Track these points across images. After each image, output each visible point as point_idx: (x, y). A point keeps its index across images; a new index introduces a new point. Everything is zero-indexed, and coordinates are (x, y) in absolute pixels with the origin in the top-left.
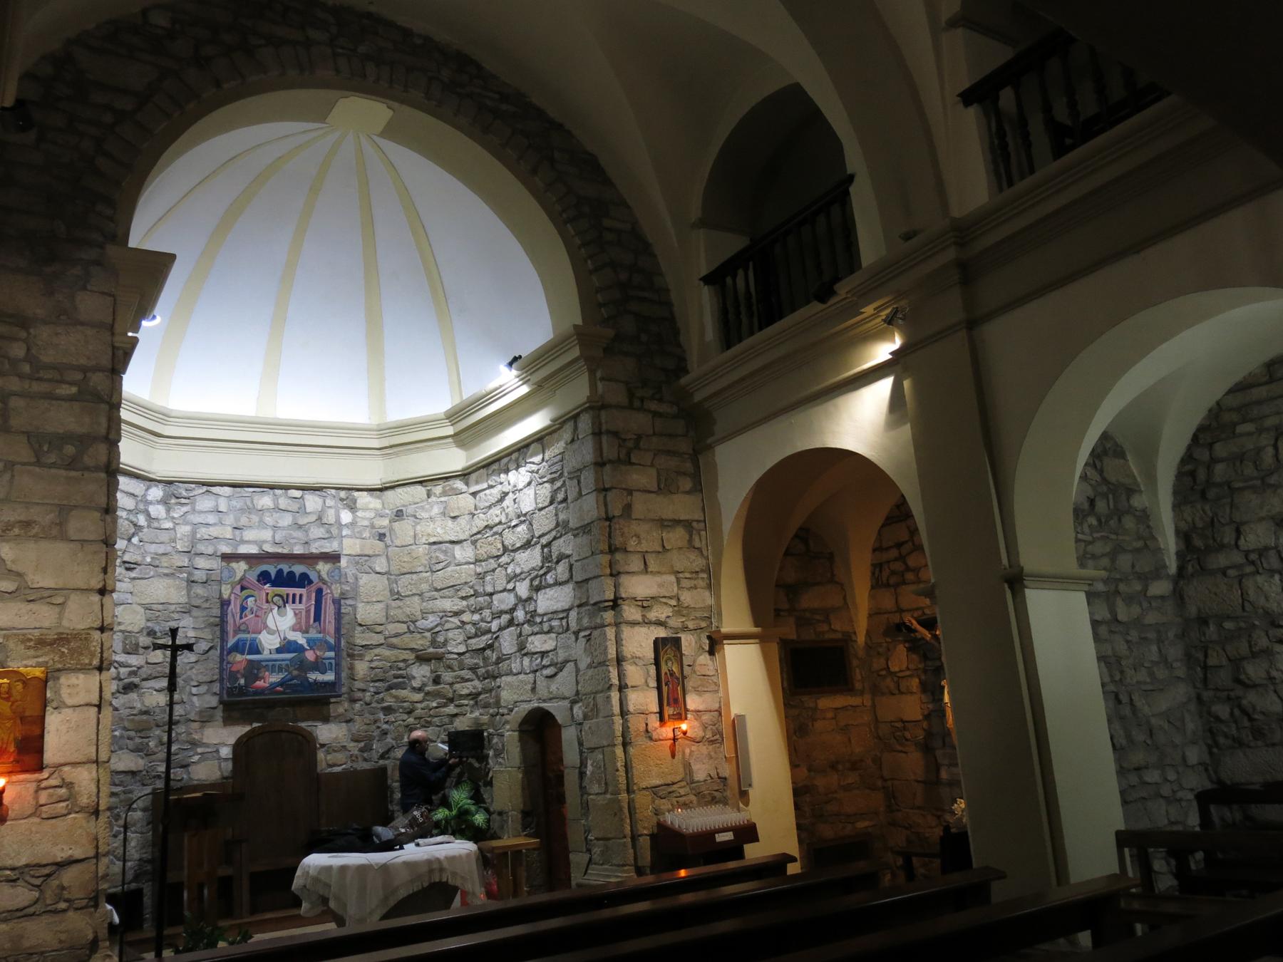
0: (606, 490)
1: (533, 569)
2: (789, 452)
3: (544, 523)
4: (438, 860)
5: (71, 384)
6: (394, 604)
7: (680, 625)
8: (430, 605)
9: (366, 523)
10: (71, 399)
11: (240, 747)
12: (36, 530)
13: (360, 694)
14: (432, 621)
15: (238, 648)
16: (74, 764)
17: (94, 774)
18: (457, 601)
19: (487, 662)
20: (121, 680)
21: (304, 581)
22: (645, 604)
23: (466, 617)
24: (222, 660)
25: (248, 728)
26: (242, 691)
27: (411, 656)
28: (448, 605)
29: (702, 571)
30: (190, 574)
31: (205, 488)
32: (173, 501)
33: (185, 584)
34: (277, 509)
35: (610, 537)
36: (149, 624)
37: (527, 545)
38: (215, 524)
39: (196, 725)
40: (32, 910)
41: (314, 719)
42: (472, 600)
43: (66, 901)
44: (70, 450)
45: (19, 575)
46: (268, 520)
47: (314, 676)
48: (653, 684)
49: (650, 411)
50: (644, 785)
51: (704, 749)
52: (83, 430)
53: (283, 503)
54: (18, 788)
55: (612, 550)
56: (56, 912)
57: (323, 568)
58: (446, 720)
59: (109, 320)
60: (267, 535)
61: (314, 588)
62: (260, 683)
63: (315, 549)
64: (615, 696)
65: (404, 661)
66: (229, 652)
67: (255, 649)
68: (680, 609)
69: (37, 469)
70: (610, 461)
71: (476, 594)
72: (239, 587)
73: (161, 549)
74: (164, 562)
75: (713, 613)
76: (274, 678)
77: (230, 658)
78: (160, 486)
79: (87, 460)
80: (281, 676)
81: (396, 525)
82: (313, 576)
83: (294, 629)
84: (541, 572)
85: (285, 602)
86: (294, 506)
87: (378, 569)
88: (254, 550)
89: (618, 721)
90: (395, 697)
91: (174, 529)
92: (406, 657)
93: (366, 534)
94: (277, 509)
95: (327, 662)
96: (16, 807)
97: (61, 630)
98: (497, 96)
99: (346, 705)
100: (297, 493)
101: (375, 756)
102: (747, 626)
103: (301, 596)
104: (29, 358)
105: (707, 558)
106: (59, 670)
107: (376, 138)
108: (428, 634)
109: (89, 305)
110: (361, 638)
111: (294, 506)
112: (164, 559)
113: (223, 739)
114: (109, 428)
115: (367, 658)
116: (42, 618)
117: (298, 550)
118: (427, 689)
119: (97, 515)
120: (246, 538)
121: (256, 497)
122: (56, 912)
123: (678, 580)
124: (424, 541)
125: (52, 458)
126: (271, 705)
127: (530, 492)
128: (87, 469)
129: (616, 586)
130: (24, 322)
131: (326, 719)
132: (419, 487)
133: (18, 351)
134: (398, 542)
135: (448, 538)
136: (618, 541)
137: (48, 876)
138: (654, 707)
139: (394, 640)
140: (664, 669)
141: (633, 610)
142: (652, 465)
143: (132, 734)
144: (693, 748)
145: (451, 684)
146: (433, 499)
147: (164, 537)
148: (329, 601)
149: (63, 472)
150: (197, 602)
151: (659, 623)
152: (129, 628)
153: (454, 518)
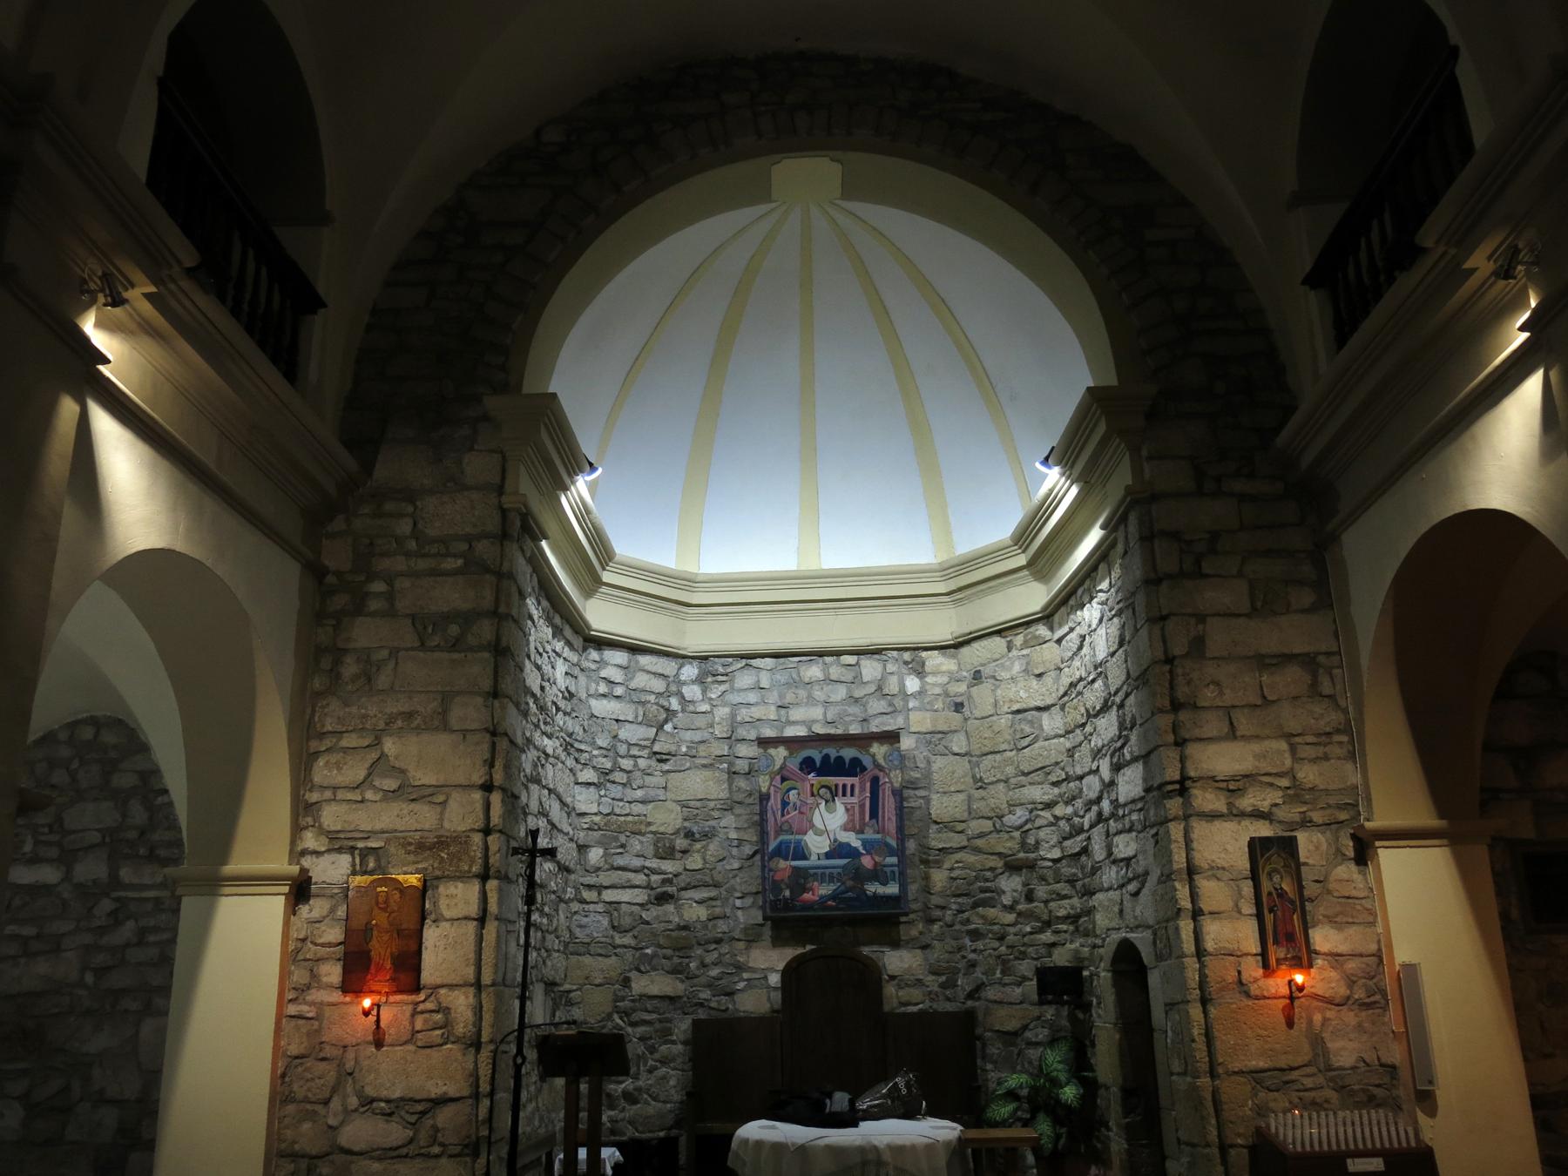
0: (1164, 618)
1: (1112, 740)
2: (1424, 528)
3: (1116, 675)
4: (875, 1148)
5: (455, 556)
6: (978, 794)
7: (1297, 818)
9: (938, 690)
11: (791, 973)
12: (418, 721)
13: (938, 913)
14: (1019, 816)
15: (781, 852)
16: (451, 987)
17: (471, 1000)
18: (1047, 787)
19: (1079, 873)
22: (1233, 786)
23: (1060, 810)
24: (763, 867)
25: (800, 951)
26: (788, 905)
27: (1000, 864)
28: (1039, 793)
29: (1338, 731)
30: (731, 764)
31: (744, 662)
32: (710, 679)
34: (828, 680)
35: (1172, 687)
36: (687, 824)
37: (1105, 708)
39: (741, 945)
40: (404, 1151)
41: (881, 944)
43: (442, 1145)
44: (454, 630)
45: (403, 772)
46: (818, 694)
47: (873, 888)
48: (1249, 908)
50: (1237, 1066)
51: (1350, 1017)
53: (835, 672)
54: (395, 1009)
55: (1176, 706)
56: (428, 1156)
57: (879, 750)
58: (1043, 951)
59: (497, 480)
60: (817, 713)
61: (868, 776)
62: (807, 896)
63: (875, 727)
64: (1186, 927)
65: (992, 869)
66: (770, 859)
67: (801, 853)
68: (1296, 793)
70: (1170, 576)
71: (1068, 779)
73: (697, 736)
74: (702, 749)
75: (1354, 801)
76: (824, 890)
77: (772, 865)
78: (695, 663)
79: (471, 640)
80: (832, 887)
81: (974, 690)
82: (867, 761)
83: (845, 828)
84: (1119, 744)
85: (834, 794)
86: (849, 677)
87: (956, 749)
88: (801, 732)
89: (1192, 964)
90: (983, 917)
92: (992, 864)
93: (939, 705)
94: (828, 680)
95: (888, 870)
96: (392, 1031)
97: (442, 832)
100: (851, 659)
101: (962, 995)
102: (1422, 815)
103: (853, 786)
104: (416, 534)
105: (1345, 711)
106: (437, 878)
108: (1017, 834)
109: (477, 466)
110: (937, 840)
112: (702, 747)
113: (770, 962)
114: (497, 600)
115: (947, 865)
116: (418, 819)
117: (855, 729)
118: (1020, 907)
119: (479, 700)
120: (791, 719)
122: (428, 1156)
123: (1293, 749)
124: (1006, 709)
125: (436, 640)
126: (826, 923)
127: (1102, 631)
128: (471, 649)
129: (1182, 760)
130: (410, 495)
131: (896, 944)
132: (997, 639)
133: (405, 527)
134: (978, 714)
136: (1182, 692)
137: (423, 1113)
138: (1253, 946)
139: (979, 842)
140: (1266, 886)
141: (1210, 796)
142: (1240, 575)
143: (669, 952)
144: (1329, 1014)
145: (1046, 902)
146: (1014, 653)
147: (701, 721)
148: (888, 792)
149: (445, 655)
150: (739, 797)
151: (1257, 815)
152: (662, 829)
153: (1040, 676)
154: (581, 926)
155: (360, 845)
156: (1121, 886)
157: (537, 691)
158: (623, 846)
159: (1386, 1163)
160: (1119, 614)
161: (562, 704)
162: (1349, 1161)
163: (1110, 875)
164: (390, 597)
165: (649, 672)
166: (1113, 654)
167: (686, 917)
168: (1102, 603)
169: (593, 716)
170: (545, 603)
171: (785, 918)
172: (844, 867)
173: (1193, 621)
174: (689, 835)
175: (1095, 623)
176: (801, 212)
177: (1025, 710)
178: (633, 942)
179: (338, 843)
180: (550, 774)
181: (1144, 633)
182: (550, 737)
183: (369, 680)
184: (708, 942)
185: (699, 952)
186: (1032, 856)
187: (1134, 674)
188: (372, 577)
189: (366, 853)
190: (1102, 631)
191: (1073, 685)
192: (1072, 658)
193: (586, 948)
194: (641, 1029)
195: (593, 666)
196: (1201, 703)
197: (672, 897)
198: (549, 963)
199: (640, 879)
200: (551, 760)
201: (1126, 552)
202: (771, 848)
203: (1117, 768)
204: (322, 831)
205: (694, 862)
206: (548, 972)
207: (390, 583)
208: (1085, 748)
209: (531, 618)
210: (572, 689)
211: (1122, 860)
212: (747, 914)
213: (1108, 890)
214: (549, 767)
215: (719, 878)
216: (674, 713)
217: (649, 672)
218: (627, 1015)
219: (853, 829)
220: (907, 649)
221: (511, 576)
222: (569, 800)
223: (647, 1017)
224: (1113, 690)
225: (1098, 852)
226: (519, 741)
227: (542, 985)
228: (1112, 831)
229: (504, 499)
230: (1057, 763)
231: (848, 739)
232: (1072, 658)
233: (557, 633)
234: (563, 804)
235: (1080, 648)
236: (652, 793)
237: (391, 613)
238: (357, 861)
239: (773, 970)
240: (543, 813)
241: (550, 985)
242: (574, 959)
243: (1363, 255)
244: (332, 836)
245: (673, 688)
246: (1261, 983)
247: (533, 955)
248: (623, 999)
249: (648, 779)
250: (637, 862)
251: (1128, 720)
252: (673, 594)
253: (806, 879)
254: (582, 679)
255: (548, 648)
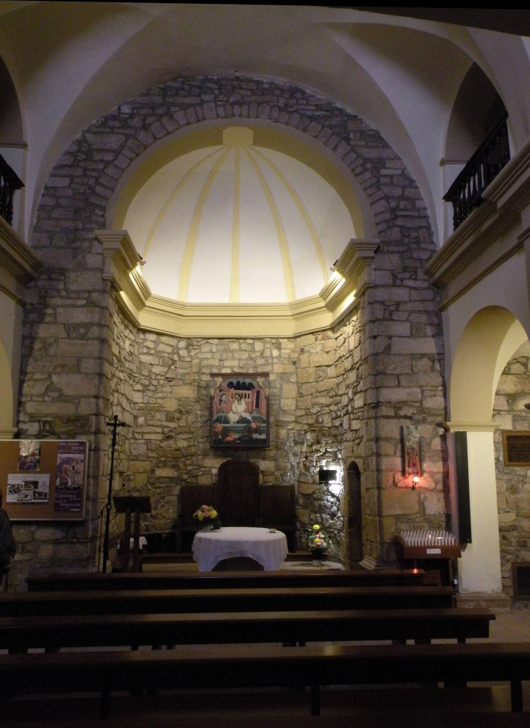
1: (354, 383)
3: (357, 356)
5: (83, 299)
6: (299, 399)
8: (316, 400)
9: (286, 356)
10: (84, 306)
11: (222, 469)
15: (218, 420)
20: (165, 434)
21: (250, 387)
23: (333, 408)
24: (211, 426)
25: (225, 460)
26: (221, 442)
31: (205, 341)
33: (196, 388)
34: (241, 350)
36: (180, 408)
38: (210, 359)
39: (200, 457)
42: (334, 399)
44: (82, 331)
46: (236, 355)
47: (255, 436)
48: (399, 454)
49: (407, 287)
52: (87, 321)
53: (243, 346)
56: (72, 543)
57: (260, 380)
60: (235, 363)
61: (255, 390)
62: (229, 439)
63: (259, 370)
67: (226, 421)
69: (68, 341)
71: (336, 395)
72: (218, 390)
73: (185, 371)
74: (187, 377)
76: (236, 436)
77: (215, 425)
78: (185, 340)
84: (356, 384)
85: (241, 397)
86: (249, 348)
88: (228, 371)
91: (191, 361)
94: (241, 350)
95: (262, 429)
98: (314, 108)
99: (274, 452)
103: (249, 394)
107: (252, 146)
108: (314, 416)
111: (249, 348)
113: (213, 465)
116: (69, 409)
117: (251, 371)
120: (225, 365)
121: (230, 344)
123: (422, 392)
126: (237, 449)
128: (89, 339)
131: (264, 459)
132: (311, 336)
134: (302, 366)
135: (324, 364)
142: (407, 320)
143: (171, 460)
146: (318, 342)
147: (186, 365)
148: (263, 398)
149: (79, 342)
152: (169, 409)
153: (327, 352)
154: (135, 449)
155: (43, 419)
156: (354, 440)
157: (117, 353)
158: (153, 416)
159: (442, 551)
160: (360, 331)
161: (128, 358)
162: (428, 550)
163: (349, 436)
164: (55, 315)
165: (165, 344)
166: (356, 348)
167: (179, 445)
168: (353, 326)
169: (141, 362)
170: (121, 316)
171: (218, 446)
172: (244, 427)
173: (387, 339)
174: (181, 412)
175: (350, 333)
176: (237, 154)
177: (321, 366)
178: (156, 456)
179: (33, 418)
180: (122, 388)
181: (367, 342)
182: (122, 372)
183: (46, 350)
184: (187, 456)
185: (183, 459)
186: (321, 425)
187: (363, 358)
188: (47, 306)
189: (45, 423)
190: (352, 337)
191: (340, 358)
192: (341, 346)
193: (136, 458)
194: (158, 490)
195: (141, 341)
196: (388, 372)
197: (173, 437)
198: (121, 465)
199: (160, 430)
200: (123, 382)
201: (363, 308)
202: (214, 419)
203: (355, 394)
204: (26, 413)
205: (182, 423)
206: (121, 468)
207: (55, 310)
208: (343, 385)
209: (115, 323)
210: (132, 351)
211: (355, 430)
212: (203, 445)
213: (348, 441)
214: (123, 385)
215: (192, 429)
216: (176, 361)
217: (165, 344)
218: (153, 484)
219: (248, 412)
220: (274, 338)
221: (107, 308)
222: (130, 398)
223: (161, 485)
224: (355, 362)
225: (346, 426)
226: (110, 376)
227: (118, 473)
228: (351, 418)
229: (104, 275)
230: (332, 389)
231: (247, 375)
232: (341, 346)
233: (126, 327)
234: (128, 399)
235: (344, 343)
236: (165, 395)
237: (55, 323)
238: (42, 426)
239: (213, 467)
240: (119, 404)
241: (121, 473)
242: (131, 462)
243: (467, 190)
244: (31, 416)
245: (175, 351)
246: (402, 482)
247: (115, 462)
248: (152, 478)
249: (164, 389)
250: (159, 423)
251: (360, 375)
252: (176, 310)
253: (228, 432)
254: (136, 347)
255: (122, 335)
